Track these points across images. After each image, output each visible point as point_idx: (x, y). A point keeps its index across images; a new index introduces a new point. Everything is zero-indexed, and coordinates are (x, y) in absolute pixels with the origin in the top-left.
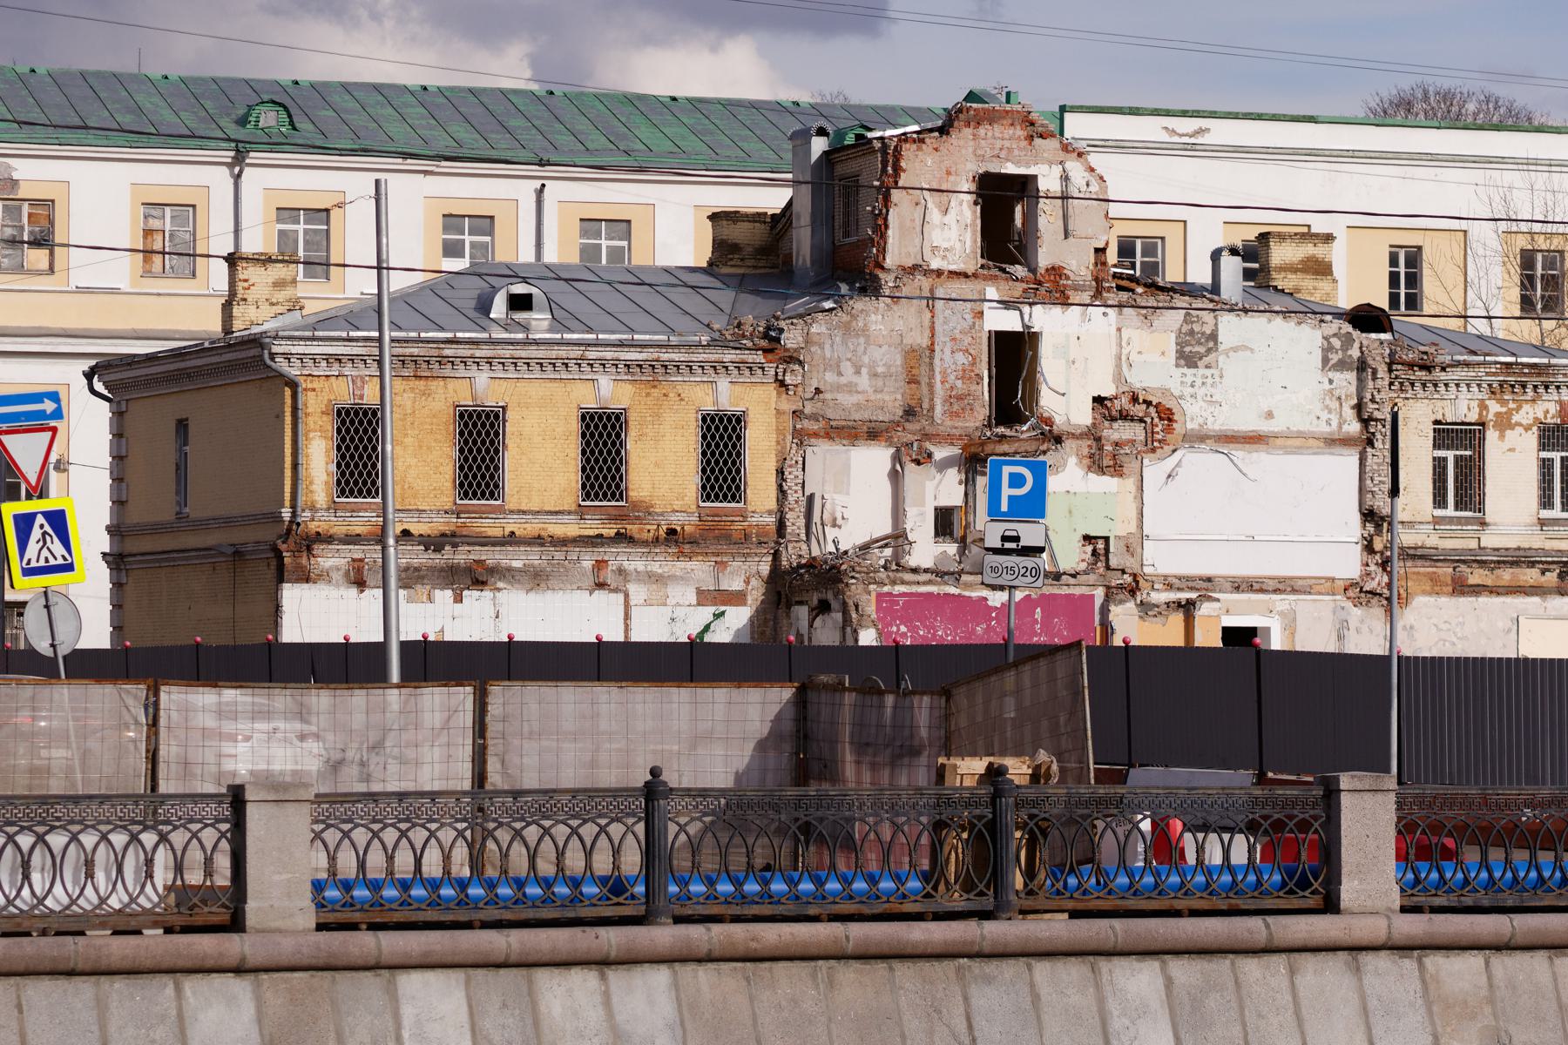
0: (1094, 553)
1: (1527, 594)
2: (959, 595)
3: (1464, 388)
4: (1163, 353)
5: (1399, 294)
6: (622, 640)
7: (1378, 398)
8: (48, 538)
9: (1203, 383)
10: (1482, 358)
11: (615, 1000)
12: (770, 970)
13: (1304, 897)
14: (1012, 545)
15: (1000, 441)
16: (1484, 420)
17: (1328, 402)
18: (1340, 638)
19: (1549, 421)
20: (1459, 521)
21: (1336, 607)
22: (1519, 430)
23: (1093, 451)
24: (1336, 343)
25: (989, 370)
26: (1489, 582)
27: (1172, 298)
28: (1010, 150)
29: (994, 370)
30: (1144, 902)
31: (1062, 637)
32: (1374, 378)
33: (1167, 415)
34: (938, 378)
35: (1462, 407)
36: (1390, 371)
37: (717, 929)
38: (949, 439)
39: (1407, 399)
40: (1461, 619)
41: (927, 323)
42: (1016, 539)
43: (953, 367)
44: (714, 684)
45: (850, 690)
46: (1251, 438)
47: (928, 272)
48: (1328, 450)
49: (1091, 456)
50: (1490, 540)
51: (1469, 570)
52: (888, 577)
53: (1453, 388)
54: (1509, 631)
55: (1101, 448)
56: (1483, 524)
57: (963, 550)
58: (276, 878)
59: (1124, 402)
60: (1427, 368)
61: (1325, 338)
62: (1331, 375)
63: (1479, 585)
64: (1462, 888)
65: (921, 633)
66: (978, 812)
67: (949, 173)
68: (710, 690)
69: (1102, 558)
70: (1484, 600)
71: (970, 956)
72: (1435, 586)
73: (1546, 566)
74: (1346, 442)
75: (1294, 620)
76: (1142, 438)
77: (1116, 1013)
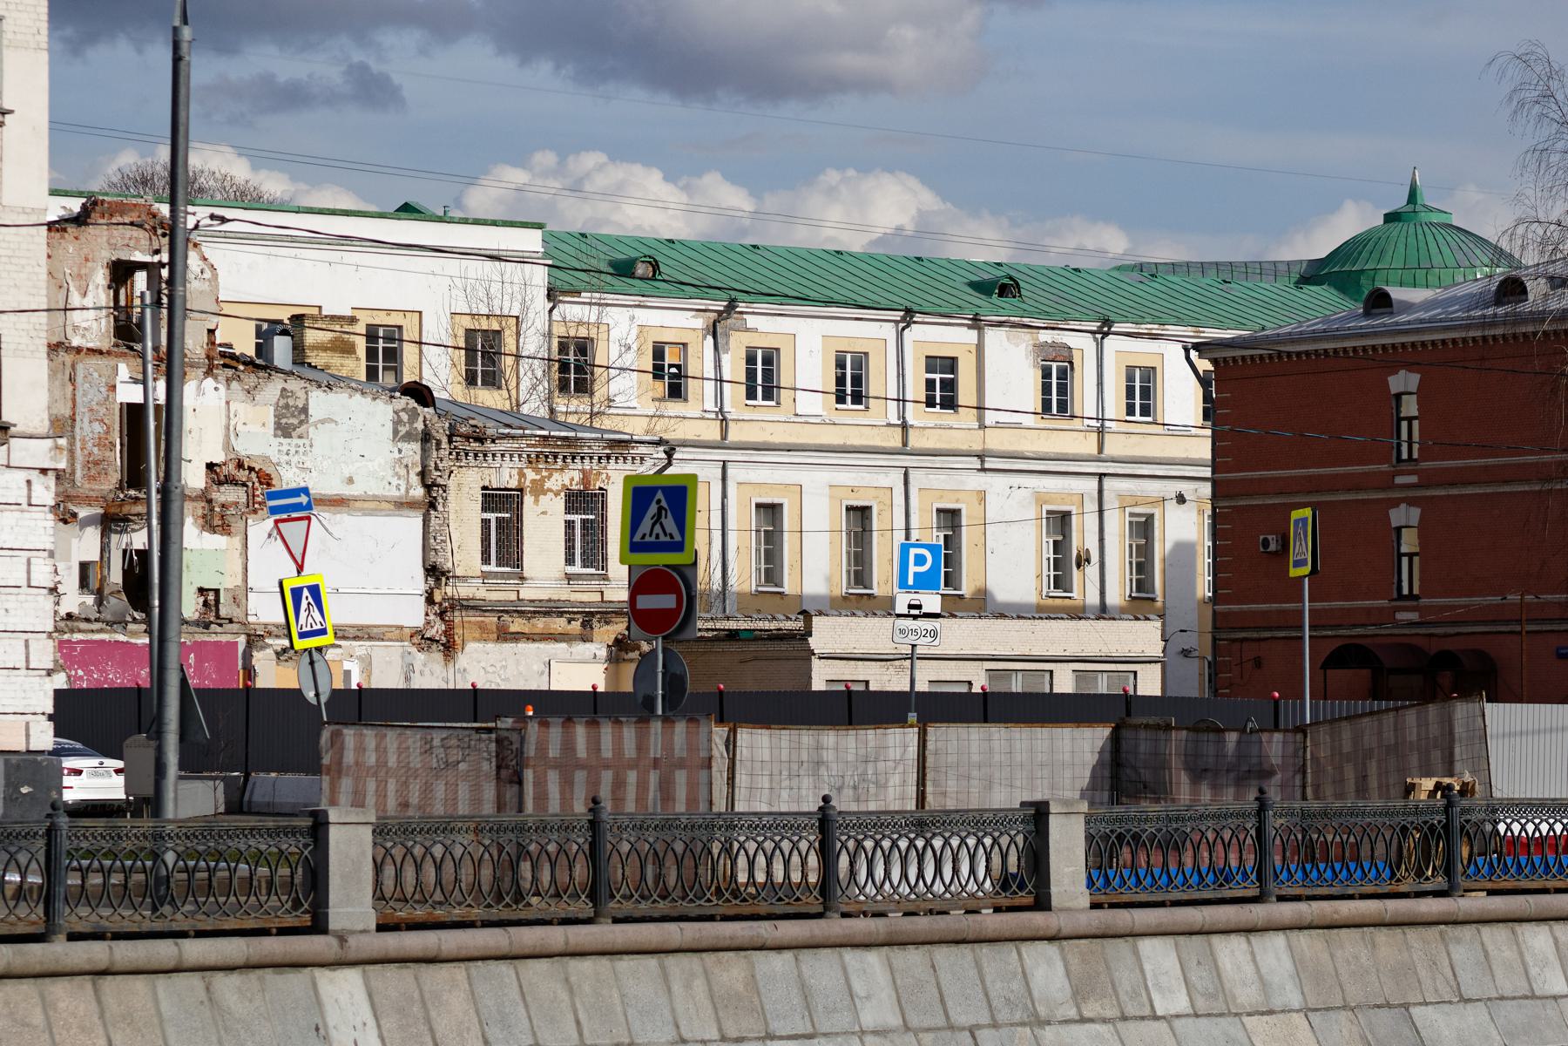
0: (206, 604)
1: (556, 640)
2: (127, 643)
3: (507, 458)
4: (264, 424)
5: (378, 367)
6: (1159, 693)
7: (440, 465)
8: (663, 512)
9: (297, 452)
10: (521, 431)
11: (1258, 958)
12: (1338, 934)
13: (1245, 888)
14: (916, 612)
15: (135, 503)
16: (522, 486)
17: (397, 469)
18: (407, 679)
19: (574, 487)
20: (502, 575)
21: (404, 652)
22: (550, 495)
23: (205, 512)
24: (404, 417)
25: (121, 438)
26: (526, 630)
27: (270, 375)
28: (138, 240)
29: (126, 439)
30: (1529, 883)
31: (212, 680)
32: (438, 448)
33: (266, 480)
34: (78, 445)
35: (505, 475)
36: (450, 442)
37: (1315, 905)
38: (88, 501)
39: (461, 467)
40: (504, 663)
41: (69, 395)
42: (919, 607)
43: (91, 435)
44: (1063, 725)
45: (1177, 728)
46: (335, 501)
47: (69, 349)
48: (397, 513)
49: (204, 516)
50: (527, 593)
51: (510, 619)
52: (67, 625)
53: (498, 458)
54: (542, 673)
55: (212, 510)
56: (522, 578)
57: (100, 602)
58: (1066, 870)
59: (231, 469)
60: (481, 440)
61: (395, 412)
62: (400, 445)
63: (518, 633)
64: (1168, 886)
65: (95, 676)
66: (1410, 819)
67: (87, 260)
68: (1060, 729)
69: (213, 608)
70: (523, 647)
71: (1446, 923)
72: (484, 634)
73: (572, 616)
74: (411, 505)
75: (370, 664)
76: (244, 500)
77: (1531, 964)
